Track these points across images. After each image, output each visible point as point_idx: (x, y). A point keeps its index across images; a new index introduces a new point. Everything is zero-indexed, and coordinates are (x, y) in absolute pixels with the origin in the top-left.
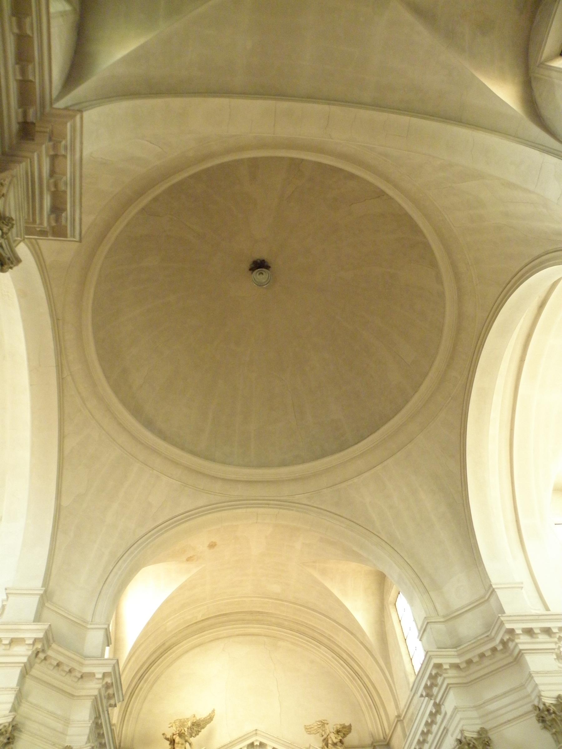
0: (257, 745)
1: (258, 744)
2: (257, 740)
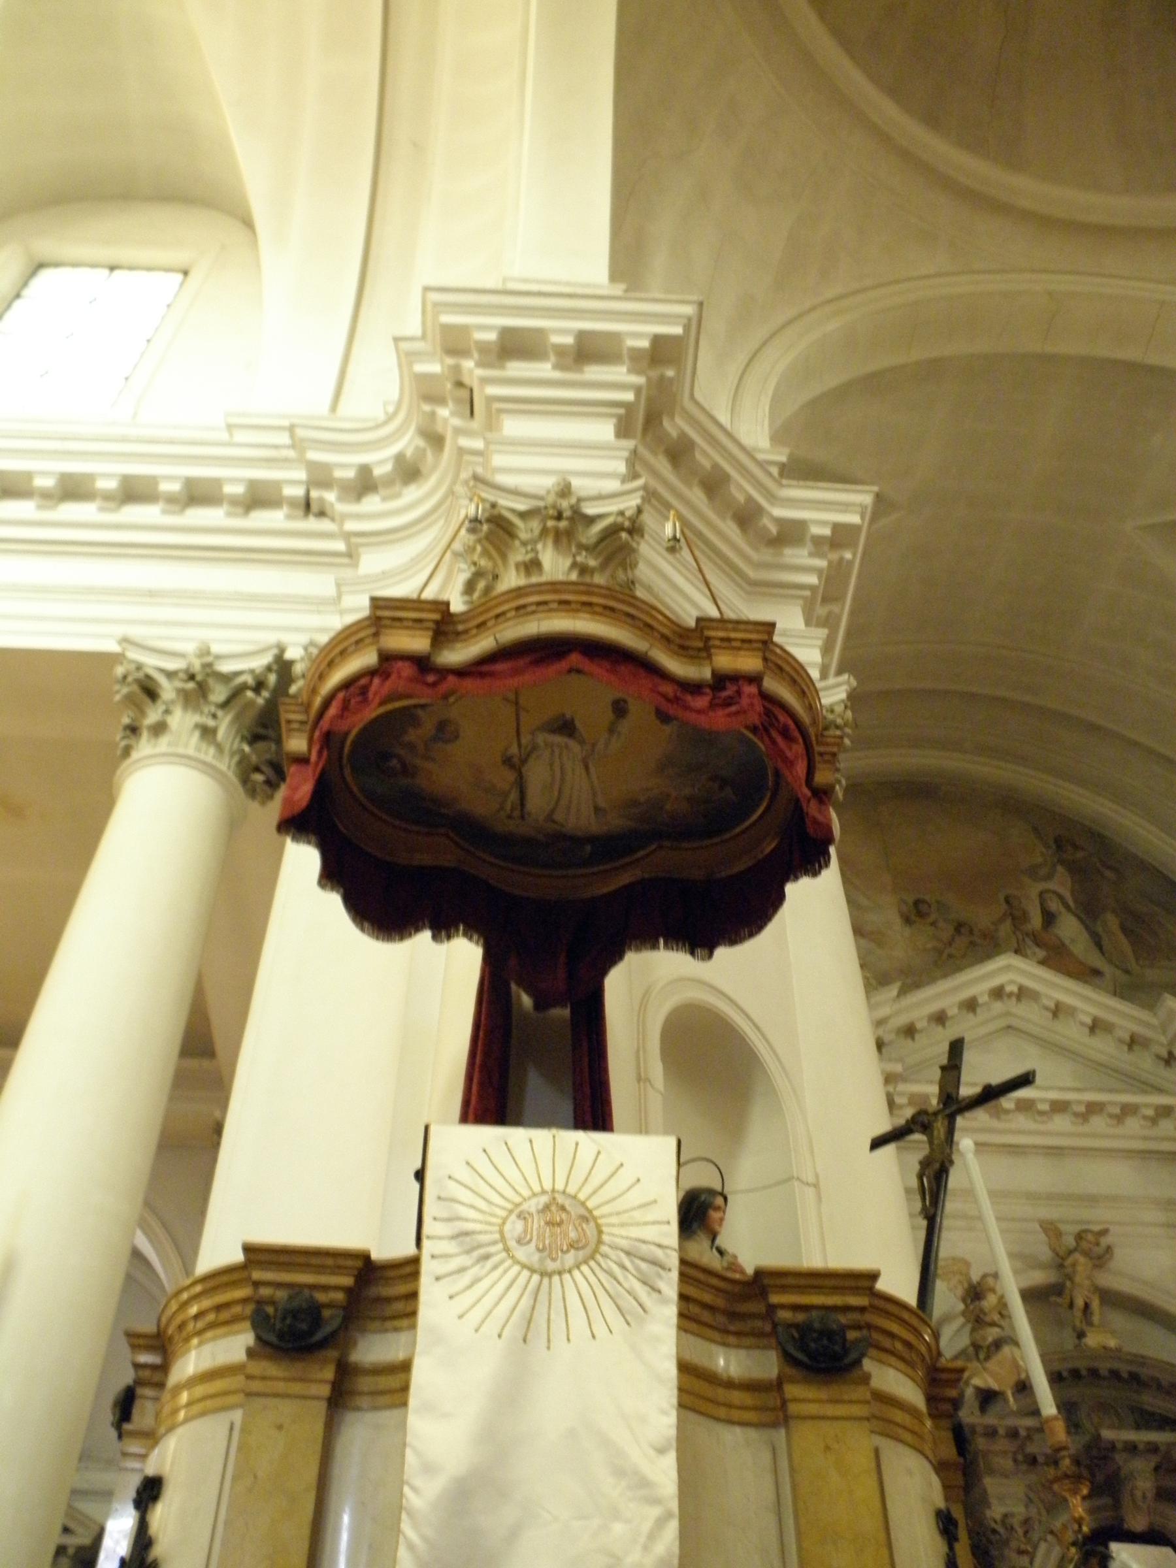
0: (1010, 995)
1: (1015, 989)
2: (1012, 982)
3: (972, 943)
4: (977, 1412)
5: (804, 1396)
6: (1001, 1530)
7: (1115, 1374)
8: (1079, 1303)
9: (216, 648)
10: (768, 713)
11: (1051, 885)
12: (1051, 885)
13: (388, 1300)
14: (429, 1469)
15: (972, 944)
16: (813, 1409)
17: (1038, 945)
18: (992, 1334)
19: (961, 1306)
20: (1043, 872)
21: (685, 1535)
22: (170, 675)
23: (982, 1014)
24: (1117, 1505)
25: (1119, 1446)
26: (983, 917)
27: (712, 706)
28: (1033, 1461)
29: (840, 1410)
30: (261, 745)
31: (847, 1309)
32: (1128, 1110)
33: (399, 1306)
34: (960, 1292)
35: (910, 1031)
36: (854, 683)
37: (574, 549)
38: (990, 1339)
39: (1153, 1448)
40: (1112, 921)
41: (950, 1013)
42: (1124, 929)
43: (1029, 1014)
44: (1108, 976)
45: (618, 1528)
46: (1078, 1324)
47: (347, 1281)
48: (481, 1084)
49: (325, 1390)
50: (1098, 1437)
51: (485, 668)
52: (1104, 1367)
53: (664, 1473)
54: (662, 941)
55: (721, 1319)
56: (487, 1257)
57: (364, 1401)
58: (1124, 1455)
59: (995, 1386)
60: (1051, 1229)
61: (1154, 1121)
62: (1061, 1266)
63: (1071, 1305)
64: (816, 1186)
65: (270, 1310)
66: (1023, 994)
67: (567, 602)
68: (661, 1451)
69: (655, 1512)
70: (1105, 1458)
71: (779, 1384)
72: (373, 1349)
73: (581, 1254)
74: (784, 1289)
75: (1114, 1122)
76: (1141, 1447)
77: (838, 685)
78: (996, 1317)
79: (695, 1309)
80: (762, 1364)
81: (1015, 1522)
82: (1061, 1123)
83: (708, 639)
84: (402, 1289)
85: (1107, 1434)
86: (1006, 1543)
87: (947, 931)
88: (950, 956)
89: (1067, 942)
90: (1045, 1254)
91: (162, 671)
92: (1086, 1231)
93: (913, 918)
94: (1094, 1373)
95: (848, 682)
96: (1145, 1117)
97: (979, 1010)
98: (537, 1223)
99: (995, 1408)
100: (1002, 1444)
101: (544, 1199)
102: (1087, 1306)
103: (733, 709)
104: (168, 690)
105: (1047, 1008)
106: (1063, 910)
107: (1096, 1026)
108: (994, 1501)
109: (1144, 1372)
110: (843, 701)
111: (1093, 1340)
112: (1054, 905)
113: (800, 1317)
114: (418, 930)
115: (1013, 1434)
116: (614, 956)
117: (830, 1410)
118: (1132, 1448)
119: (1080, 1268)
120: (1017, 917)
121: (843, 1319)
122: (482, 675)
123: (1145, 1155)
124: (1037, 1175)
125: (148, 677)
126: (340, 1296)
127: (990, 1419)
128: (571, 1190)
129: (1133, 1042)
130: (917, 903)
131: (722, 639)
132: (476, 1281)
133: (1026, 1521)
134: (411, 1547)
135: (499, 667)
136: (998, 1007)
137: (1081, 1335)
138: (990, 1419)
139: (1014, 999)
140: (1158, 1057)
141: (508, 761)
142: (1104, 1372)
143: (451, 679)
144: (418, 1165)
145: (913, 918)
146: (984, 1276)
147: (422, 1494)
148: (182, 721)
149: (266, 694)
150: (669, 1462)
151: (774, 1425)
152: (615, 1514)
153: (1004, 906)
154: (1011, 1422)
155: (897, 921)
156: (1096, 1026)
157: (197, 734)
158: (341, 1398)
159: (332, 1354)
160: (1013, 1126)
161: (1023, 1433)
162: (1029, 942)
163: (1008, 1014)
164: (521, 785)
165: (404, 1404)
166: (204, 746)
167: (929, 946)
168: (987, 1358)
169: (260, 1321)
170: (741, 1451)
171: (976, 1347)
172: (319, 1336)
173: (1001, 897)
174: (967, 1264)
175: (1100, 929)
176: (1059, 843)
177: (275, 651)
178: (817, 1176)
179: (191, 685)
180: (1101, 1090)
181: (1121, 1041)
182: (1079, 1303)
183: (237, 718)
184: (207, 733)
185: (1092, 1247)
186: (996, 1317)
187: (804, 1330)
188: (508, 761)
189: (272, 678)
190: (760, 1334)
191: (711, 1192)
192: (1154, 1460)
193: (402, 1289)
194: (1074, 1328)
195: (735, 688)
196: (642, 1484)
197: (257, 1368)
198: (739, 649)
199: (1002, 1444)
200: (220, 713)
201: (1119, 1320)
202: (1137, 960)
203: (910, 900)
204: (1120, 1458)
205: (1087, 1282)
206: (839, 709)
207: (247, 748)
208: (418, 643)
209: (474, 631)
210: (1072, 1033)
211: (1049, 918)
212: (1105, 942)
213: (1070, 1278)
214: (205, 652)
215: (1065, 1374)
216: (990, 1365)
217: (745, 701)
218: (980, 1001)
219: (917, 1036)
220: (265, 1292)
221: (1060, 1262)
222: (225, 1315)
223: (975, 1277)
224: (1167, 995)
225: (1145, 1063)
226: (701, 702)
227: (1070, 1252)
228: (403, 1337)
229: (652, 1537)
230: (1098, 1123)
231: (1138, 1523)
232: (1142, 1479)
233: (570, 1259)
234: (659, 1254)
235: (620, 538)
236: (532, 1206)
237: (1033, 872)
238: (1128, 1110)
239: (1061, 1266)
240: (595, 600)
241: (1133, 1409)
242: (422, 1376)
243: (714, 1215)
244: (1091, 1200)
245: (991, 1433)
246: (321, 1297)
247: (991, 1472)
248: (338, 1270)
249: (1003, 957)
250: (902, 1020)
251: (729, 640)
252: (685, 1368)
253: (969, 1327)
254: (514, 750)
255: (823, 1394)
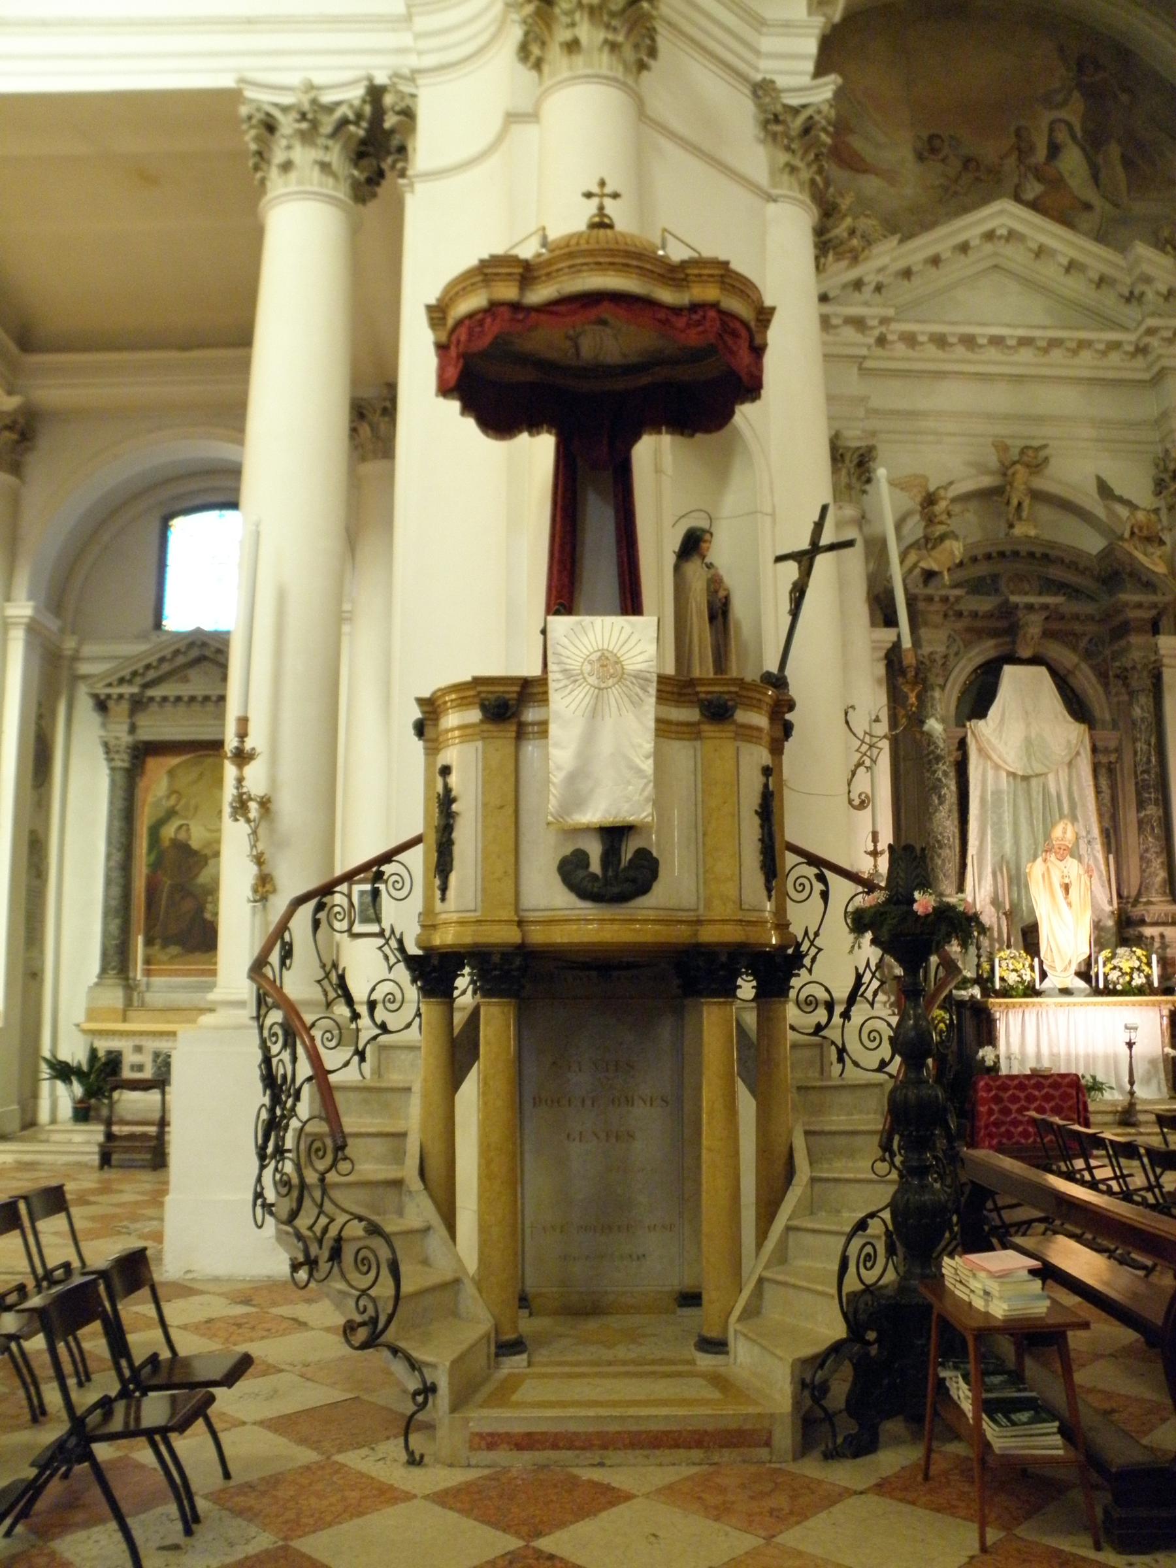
0: (1000, 237)
3: (977, 179)
4: (921, 586)
5: (708, 729)
6: (928, 662)
7: (1032, 555)
8: (1015, 502)
9: (318, 79)
10: (723, 323)
11: (1063, 114)
12: (1063, 114)
13: (535, 694)
14: (559, 768)
15: (977, 179)
16: (712, 734)
17: (1039, 180)
18: (939, 530)
19: (919, 508)
20: (1059, 98)
21: (656, 786)
22: (285, 109)
23: (973, 256)
24: (1014, 642)
25: (1021, 606)
26: (989, 150)
27: (688, 326)
28: (959, 614)
29: (723, 735)
30: (365, 162)
31: (730, 692)
32: (1083, 344)
33: (540, 697)
34: (919, 499)
35: (907, 273)
36: (840, 80)
37: (606, 18)
38: (937, 534)
39: (1045, 607)
40: (1114, 150)
41: (944, 256)
42: (1127, 163)
43: (1015, 256)
44: (1098, 209)
45: (630, 788)
46: (1011, 516)
47: (517, 689)
48: (563, 518)
49: (513, 734)
50: (1007, 601)
51: (555, 308)
52: (1024, 549)
53: (648, 766)
54: (664, 428)
55: (676, 697)
56: (575, 681)
57: (531, 736)
58: (1025, 611)
59: (935, 567)
60: (1001, 447)
61: (1104, 353)
62: (1005, 475)
63: (1008, 503)
64: (773, 515)
65: (487, 703)
66: (1012, 236)
67: (599, 264)
68: (647, 757)
69: (645, 781)
70: (1011, 613)
71: (698, 723)
72: (531, 715)
73: (615, 680)
74: (703, 685)
75: (1070, 354)
76: (1037, 606)
77: (826, 84)
78: (944, 517)
79: (664, 695)
80: (690, 714)
81: (937, 657)
82: (1026, 355)
83: (687, 275)
84: (541, 690)
85: (1014, 599)
86: (929, 670)
87: (957, 164)
88: (956, 193)
89: (1066, 175)
90: (993, 461)
91: (276, 105)
92: (1027, 447)
93: (926, 154)
94: (1016, 554)
95: (834, 82)
96: (1097, 351)
97: (970, 252)
98: (597, 665)
99: (934, 583)
100: (937, 606)
101: (599, 654)
102: (1020, 504)
103: (701, 328)
104: (287, 124)
105: (1030, 250)
106: (1070, 141)
107: (1072, 267)
108: (924, 644)
109: (1053, 553)
110: (827, 101)
111: (1019, 530)
112: (1062, 136)
113: (709, 697)
114: (520, 432)
115: (945, 599)
116: (636, 437)
117: (717, 734)
118: (1030, 607)
119: (1018, 476)
120: (1023, 150)
121: (727, 697)
122: (551, 313)
123: (1092, 381)
124: (999, 399)
125: (268, 115)
126: (515, 696)
127: (929, 591)
128: (610, 649)
129: (1102, 282)
130: (932, 138)
131: (696, 276)
132: (572, 691)
133: (946, 656)
134: (554, 796)
135: (562, 309)
136: (988, 248)
137: (1011, 526)
138: (929, 591)
139: (1003, 241)
140: (1121, 296)
141: (568, 337)
142: (1023, 553)
143: (533, 314)
144: (541, 626)
145: (926, 154)
146: (938, 488)
147: (557, 777)
148: (303, 156)
149: (364, 124)
150: (651, 761)
151: (695, 739)
152: (629, 783)
153: (1013, 140)
154: (943, 592)
155: (909, 156)
156: (1072, 267)
157: (317, 168)
158: (521, 734)
159: (514, 720)
160: (983, 357)
161: (952, 599)
162: (1030, 176)
163: (996, 254)
164: (577, 347)
165: (547, 737)
166: (324, 178)
167: (937, 183)
168: (933, 548)
169: (484, 708)
170: (682, 753)
171: (927, 539)
172: (509, 714)
173: (1012, 129)
174: (925, 478)
175: (1100, 160)
176: (1081, 64)
177: (365, 83)
178: (774, 507)
179: (304, 126)
180: (1064, 328)
181: (1091, 281)
182: (1015, 502)
183: (345, 147)
184: (325, 167)
185: (1034, 459)
186: (944, 517)
187: (710, 702)
188: (568, 337)
189: (368, 109)
190: (692, 702)
191: (704, 531)
192: (1045, 614)
193: (541, 690)
194: (1008, 520)
195: (701, 313)
196: (639, 772)
197: (486, 727)
198: (707, 282)
199: (937, 606)
200: (330, 143)
201: (1045, 513)
202: (1129, 190)
203: (925, 135)
204: (1020, 614)
205: (1023, 487)
206: (825, 108)
207: (356, 173)
208: (508, 292)
209: (544, 278)
210: (1050, 272)
211: (1054, 150)
212: (1103, 175)
213: (1011, 484)
214: (310, 87)
215: (994, 555)
216: (934, 553)
217: (708, 324)
218: (972, 244)
219: (913, 278)
220: (483, 695)
221: (1005, 470)
222: (465, 701)
223: (932, 489)
224: (1137, 242)
225: (1109, 301)
226: (680, 323)
227: (1014, 463)
228: (543, 710)
229: (643, 790)
230: (1057, 354)
231: (1026, 653)
232: (1033, 626)
233: (610, 682)
234: (648, 675)
235: (642, 8)
236: (594, 657)
237: (1048, 101)
238: (1083, 344)
239: (1005, 475)
240: (617, 260)
241: (1039, 577)
242: (553, 729)
243: (704, 545)
244: (1040, 419)
245: (930, 599)
246: (507, 696)
247: (926, 624)
248: (512, 684)
249: (998, 202)
250: (901, 264)
251: (700, 275)
252: (658, 721)
253: (923, 524)
254: (571, 332)
255: (716, 729)
